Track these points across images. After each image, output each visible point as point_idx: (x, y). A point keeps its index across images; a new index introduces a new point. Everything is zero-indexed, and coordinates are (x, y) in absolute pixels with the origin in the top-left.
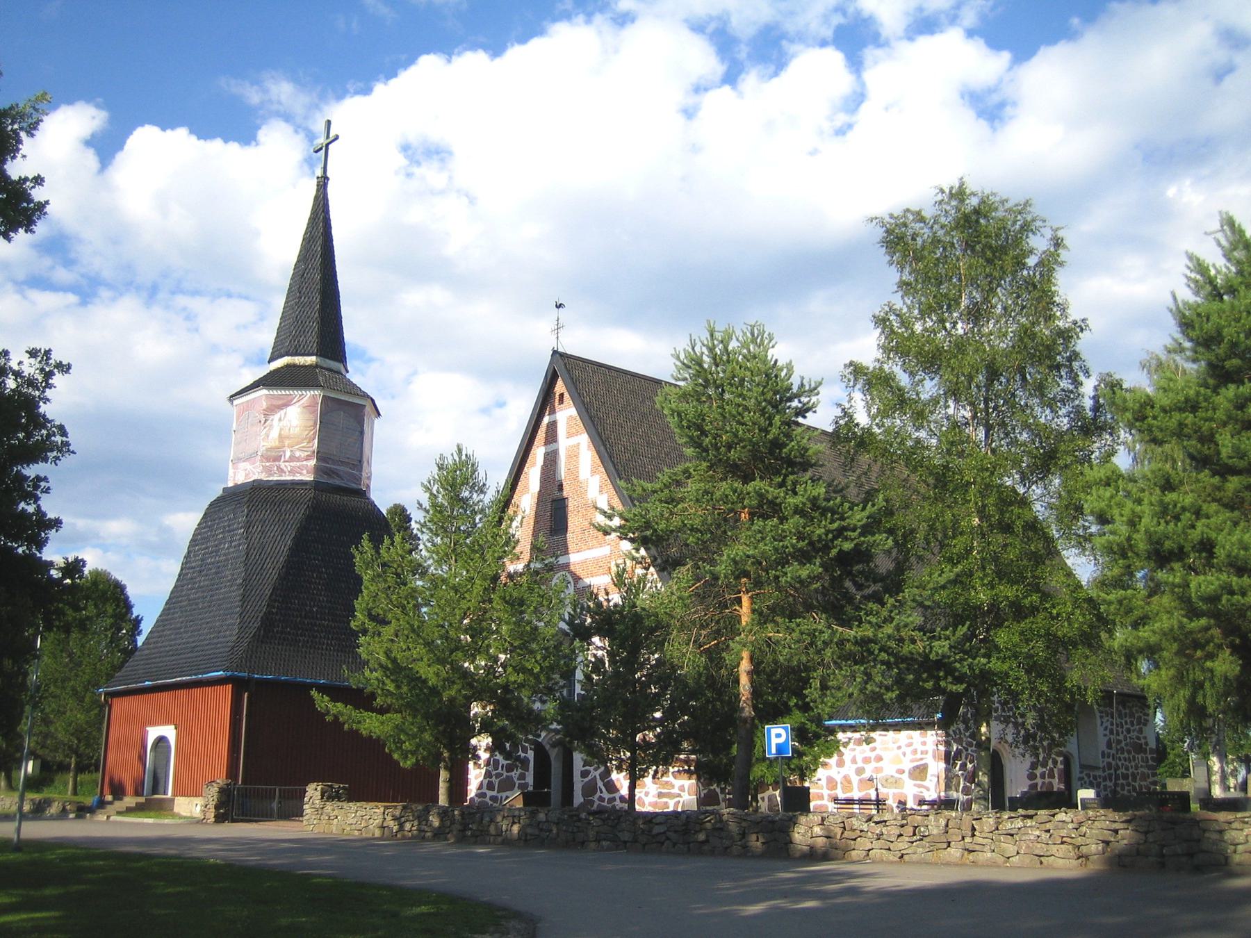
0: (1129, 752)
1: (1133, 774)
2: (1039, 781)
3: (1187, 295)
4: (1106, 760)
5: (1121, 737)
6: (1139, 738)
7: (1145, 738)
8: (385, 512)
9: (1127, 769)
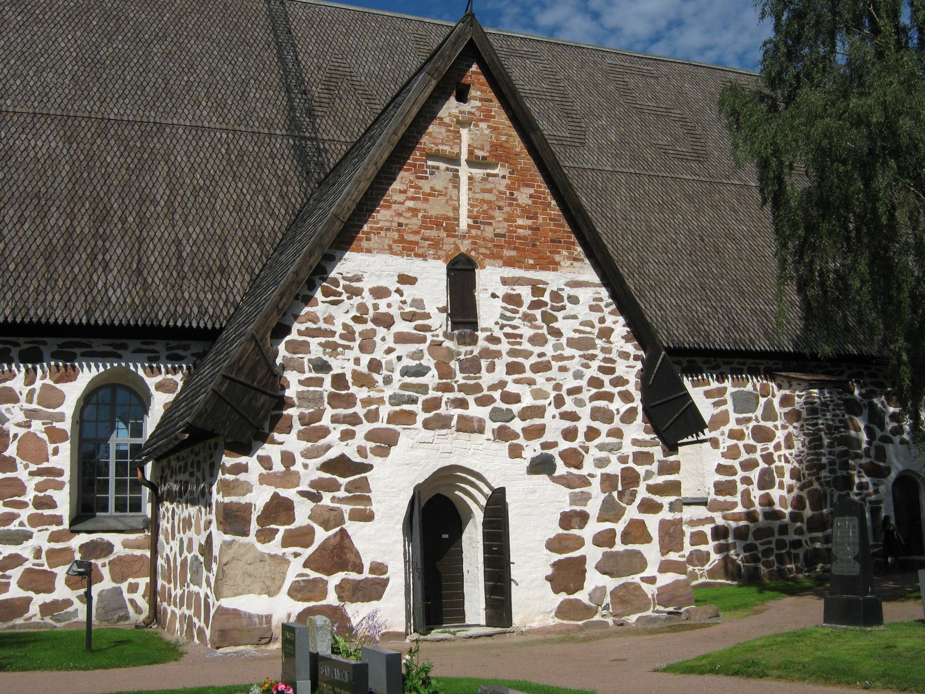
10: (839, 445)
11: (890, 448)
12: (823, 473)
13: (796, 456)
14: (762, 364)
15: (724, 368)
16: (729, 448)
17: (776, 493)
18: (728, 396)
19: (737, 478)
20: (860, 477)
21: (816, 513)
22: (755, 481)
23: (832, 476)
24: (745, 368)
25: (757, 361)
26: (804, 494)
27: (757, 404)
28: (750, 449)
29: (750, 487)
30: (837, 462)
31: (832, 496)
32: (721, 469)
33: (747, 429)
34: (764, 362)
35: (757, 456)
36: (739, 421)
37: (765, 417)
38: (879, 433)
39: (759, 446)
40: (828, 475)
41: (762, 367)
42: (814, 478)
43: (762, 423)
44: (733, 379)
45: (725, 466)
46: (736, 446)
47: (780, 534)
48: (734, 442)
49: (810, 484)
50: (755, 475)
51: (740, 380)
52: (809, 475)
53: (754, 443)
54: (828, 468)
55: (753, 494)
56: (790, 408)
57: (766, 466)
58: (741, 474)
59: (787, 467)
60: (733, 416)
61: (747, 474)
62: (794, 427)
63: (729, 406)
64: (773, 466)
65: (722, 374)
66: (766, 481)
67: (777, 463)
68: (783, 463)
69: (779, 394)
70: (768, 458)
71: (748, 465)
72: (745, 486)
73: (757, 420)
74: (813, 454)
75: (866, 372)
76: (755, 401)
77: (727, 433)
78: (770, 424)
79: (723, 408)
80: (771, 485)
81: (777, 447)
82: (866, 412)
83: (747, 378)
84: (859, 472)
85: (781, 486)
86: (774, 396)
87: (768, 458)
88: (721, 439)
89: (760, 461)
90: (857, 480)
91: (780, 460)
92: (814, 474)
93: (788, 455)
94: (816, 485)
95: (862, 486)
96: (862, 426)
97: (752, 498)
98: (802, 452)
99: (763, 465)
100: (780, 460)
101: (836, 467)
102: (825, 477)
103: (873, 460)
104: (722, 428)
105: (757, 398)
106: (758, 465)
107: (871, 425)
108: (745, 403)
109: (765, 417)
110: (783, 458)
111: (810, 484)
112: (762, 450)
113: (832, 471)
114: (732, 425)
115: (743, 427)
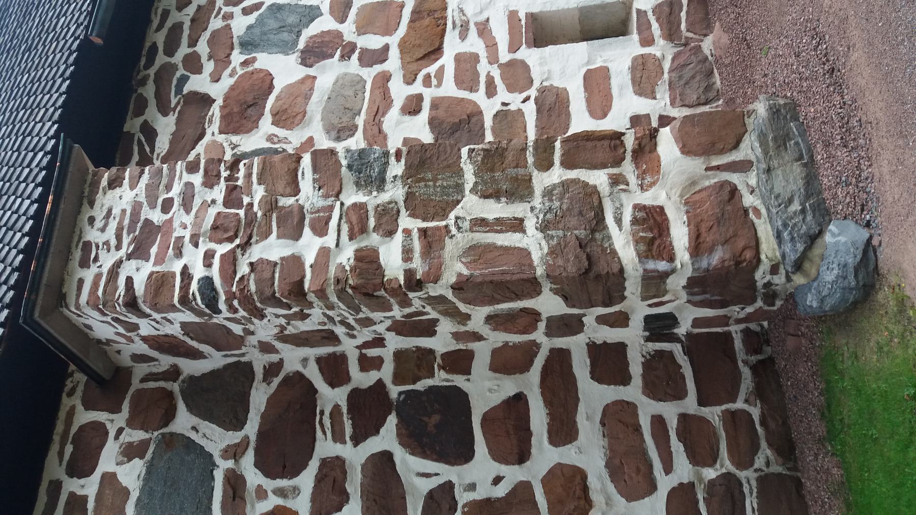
10: (296, 191)
14: (71, 413)
23: (406, 221)
27: (190, 444)
31: (480, 223)
39: (326, 447)
53: (313, 466)
67: (386, 372)
75: (161, 59)
87: (367, 410)
89: (374, 445)
91: (378, 363)
97: (501, 491)
99: (386, 438)
100: (378, 363)
102: (407, 254)
106: (386, 458)
112: (338, 437)
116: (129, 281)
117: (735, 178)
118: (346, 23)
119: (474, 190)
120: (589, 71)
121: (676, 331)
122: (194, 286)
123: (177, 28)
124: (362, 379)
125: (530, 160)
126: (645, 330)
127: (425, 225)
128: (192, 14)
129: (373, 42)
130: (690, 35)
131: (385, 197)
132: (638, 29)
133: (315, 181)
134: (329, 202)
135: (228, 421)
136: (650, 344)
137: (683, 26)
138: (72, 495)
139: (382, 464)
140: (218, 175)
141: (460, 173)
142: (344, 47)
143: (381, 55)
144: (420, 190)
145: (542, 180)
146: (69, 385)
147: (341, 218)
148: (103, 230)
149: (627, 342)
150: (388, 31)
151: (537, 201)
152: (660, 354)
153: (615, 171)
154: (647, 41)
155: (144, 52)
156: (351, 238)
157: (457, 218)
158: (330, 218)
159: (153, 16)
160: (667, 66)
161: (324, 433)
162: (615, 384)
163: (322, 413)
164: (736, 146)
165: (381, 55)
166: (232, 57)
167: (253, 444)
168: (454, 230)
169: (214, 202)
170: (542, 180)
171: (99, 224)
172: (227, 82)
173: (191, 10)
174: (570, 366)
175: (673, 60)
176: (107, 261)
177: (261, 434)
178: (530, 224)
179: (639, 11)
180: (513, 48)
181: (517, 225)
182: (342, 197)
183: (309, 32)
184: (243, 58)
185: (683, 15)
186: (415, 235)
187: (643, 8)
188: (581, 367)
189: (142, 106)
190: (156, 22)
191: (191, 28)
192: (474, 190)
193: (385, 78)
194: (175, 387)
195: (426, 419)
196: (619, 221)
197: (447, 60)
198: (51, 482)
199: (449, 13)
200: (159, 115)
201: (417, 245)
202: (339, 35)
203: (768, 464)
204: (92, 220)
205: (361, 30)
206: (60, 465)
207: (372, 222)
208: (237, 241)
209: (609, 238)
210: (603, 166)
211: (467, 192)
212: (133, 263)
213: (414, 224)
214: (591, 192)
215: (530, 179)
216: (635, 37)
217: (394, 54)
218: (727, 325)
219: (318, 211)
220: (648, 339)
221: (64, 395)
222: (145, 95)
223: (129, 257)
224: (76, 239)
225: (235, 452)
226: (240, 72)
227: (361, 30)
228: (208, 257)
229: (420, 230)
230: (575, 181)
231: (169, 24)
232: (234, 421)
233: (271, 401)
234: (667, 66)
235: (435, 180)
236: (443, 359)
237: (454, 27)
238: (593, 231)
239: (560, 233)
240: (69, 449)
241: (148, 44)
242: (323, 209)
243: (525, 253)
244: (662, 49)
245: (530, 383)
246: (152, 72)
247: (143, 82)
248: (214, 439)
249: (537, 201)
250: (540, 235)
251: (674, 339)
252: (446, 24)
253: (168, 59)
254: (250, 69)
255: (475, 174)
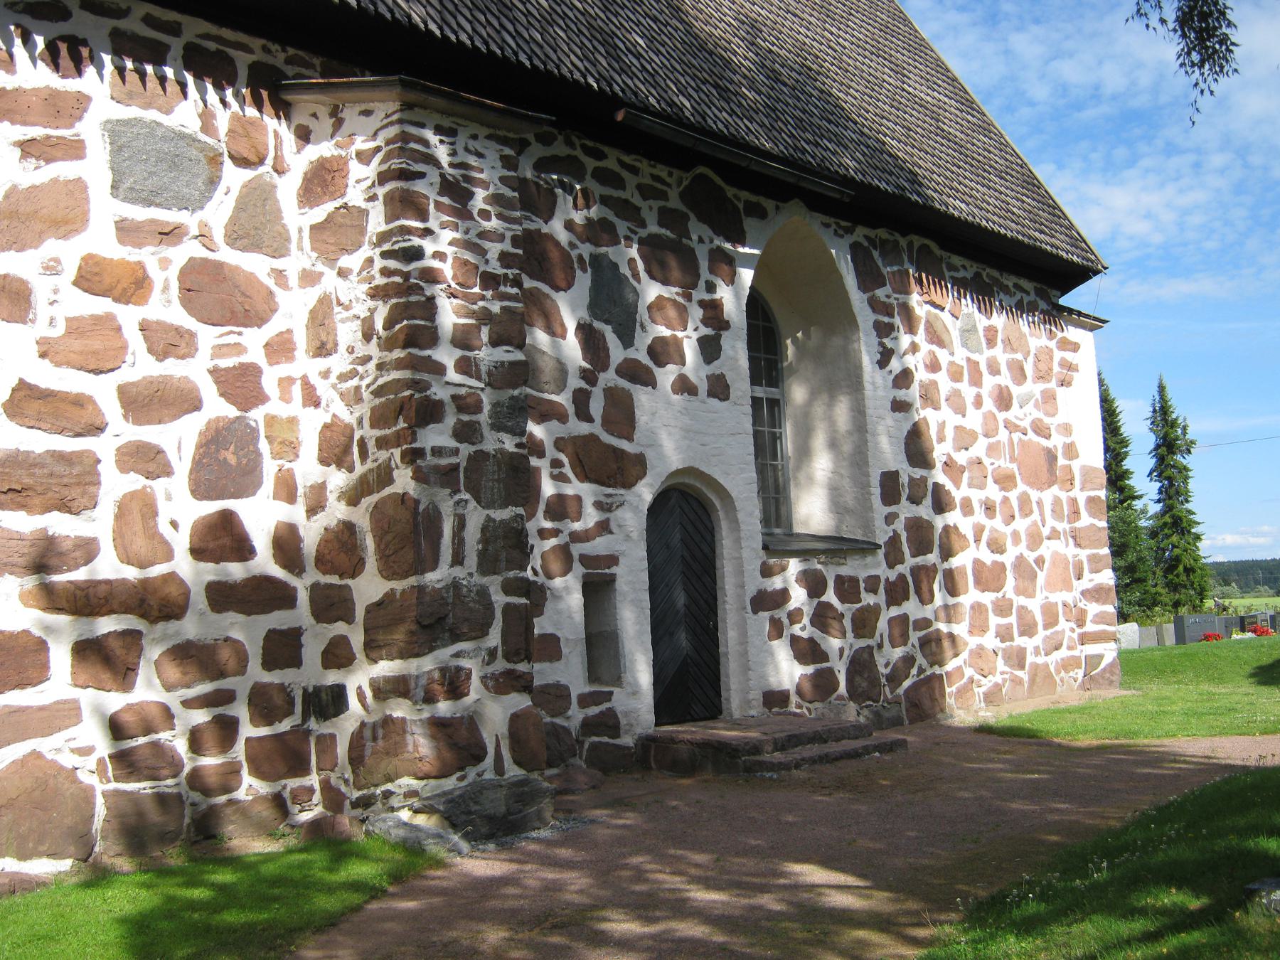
0: (1005, 481)
1: (1020, 561)
2: (1114, 678)
3: (1131, 482)
4: (905, 510)
5: (973, 420)
6: (1041, 430)
7: (1066, 429)
8: (536, 632)
9: (996, 546)
10: (495, 343)
11: (642, 397)
12: (436, 436)
13: (343, 377)
14: (248, 50)
15: (83, 23)
16: (76, 327)
17: (260, 516)
18: (90, 129)
19: (104, 447)
20: (559, 478)
21: (399, 585)
22: (182, 466)
23: (466, 449)
24: (176, 46)
25: (227, 33)
26: (361, 516)
27: (213, 182)
28: (167, 342)
29: (159, 486)
30: (486, 399)
31: (461, 524)
32: (28, 402)
33: (164, 266)
34: (256, 43)
35: (195, 370)
36: (126, 231)
37: (240, 236)
38: (617, 353)
39: (208, 336)
40: (448, 442)
41: (243, 61)
42: (397, 453)
43: (227, 255)
44: (121, 71)
45: (47, 396)
46: (108, 324)
47: (269, 663)
48: (101, 305)
49: (384, 476)
50: (179, 438)
51: (152, 82)
52: (382, 443)
53: (187, 321)
54: (451, 420)
55: (165, 513)
56: (330, 207)
57: (232, 412)
58: (123, 429)
59: (311, 425)
60: (105, 208)
61: (150, 434)
62: (343, 274)
63: (95, 168)
64: (257, 415)
65: (75, 44)
66: (226, 463)
67: (275, 407)
68: (295, 407)
69: (300, 160)
70: (241, 384)
71: (147, 402)
72: (135, 482)
73: (204, 237)
74: (399, 365)
75: (590, 163)
76: (203, 170)
77: (71, 272)
78: (256, 265)
79: (64, 170)
80: (246, 481)
81: (280, 349)
82: (584, 280)
83: (183, 86)
84: (556, 464)
85: (286, 490)
86: (279, 170)
87: (241, 384)
88: (41, 288)
89: (209, 391)
90: (548, 489)
91: (286, 398)
92: (397, 440)
93: (315, 380)
94: (404, 481)
95: (561, 509)
96: (571, 326)
97: (164, 528)
98: (366, 360)
99: (216, 407)
100: (286, 398)
101: (484, 417)
102: (437, 451)
103: (596, 428)
104: (52, 247)
105: (215, 161)
106: (196, 405)
107: (598, 325)
108: (154, 170)
109: (240, 236)
110: (297, 390)
111: (384, 476)
112: (219, 351)
113: (466, 433)
114: (100, 239)
115: (148, 256)
116: (421, 175)
117: (489, 760)
118: (615, 377)
119: (489, 519)
120: (558, 639)
121: (313, 719)
122: (416, 241)
123: (619, 183)
124: (270, 380)
125: (512, 574)
126: (315, 687)
127: (462, 470)
128: (633, 200)
129: (597, 406)
130: (586, 746)
131: (486, 431)
132: (595, 692)
133: (503, 363)
134: (484, 376)
135: (236, 228)
136: (300, 692)
137: (596, 739)
138: (167, 48)
139: (189, 401)
140: (508, 267)
141: (504, 505)
142: (592, 372)
143: (583, 414)
144: (490, 466)
145: (494, 584)
146: (275, 47)
147: (470, 387)
148: (467, 150)
149: (303, 668)
150: (607, 424)
151: (477, 579)
152: (291, 703)
153: (500, 653)
154: (585, 701)
155: (598, 145)
156: (454, 397)
157: (466, 501)
158: (471, 377)
159: (634, 157)
160: (558, 721)
161: (222, 335)
162: (263, 655)
163: (240, 334)
164: (518, 763)
165: (583, 414)
166: (588, 244)
167: (211, 255)
168: (457, 497)
169: (487, 262)
170: (494, 584)
171: (472, 144)
172: (563, 236)
173: (637, 200)
174: (280, 608)
175: (563, 727)
176: (442, 153)
177: (219, 266)
178: (459, 572)
179: (611, 693)
180: (584, 559)
181: (458, 560)
182: (488, 389)
183: (608, 331)
184: (587, 258)
185: (605, 739)
186: (454, 460)
187: (614, 698)
188: (279, 619)
189: (545, 140)
190: (627, 159)
191: (619, 198)
192: (489, 519)
193: (563, 418)
194: (267, 168)
195: (232, 448)
196: (457, 655)
197: (575, 487)
198: (179, 24)
199: (622, 491)
200: (534, 160)
201: (444, 462)
202: (605, 367)
203: (193, 804)
204: (475, 137)
205: (610, 393)
206: (198, 36)
207: (466, 418)
208: (453, 285)
209: (445, 646)
210: (504, 642)
211: (487, 512)
212: (437, 180)
213: (461, 460)
214: (481, 631)
215: (495, 573)
216: (588, 689)
217: (583, 428)
218: (319, 769)
219: (476, 365)
220: (305, 690)
221: (263, 42)
222: (555, 143)
223: (442, 176)
224: (459, 121)
225: (204, 237)
226: (574, 254)
227: (610, 393)
228: (440, 256)
229: (458, 464)
230: (492, 617)
231: (625, 174)
232: (235, 236)
233: (251, 278)
234: (558, 721)
235: (498, 481)
236: (288, 470)
237: (610, 496)
238: (451, 630)
239: (450, 600)
240: (212, 46)
241: (606, 149)
242: (478, 370)
243: (434, 566)
244: (576, 716)
245: (265, 562)
246: (578, 153)
247: (570, 144)
248: (219, 211)
249: (477, 579)
250: (450, 580)
251: (305, 718)
252: (609, 486)
253: (589, 171)
254: (576, 266)
255: (502, 521)
